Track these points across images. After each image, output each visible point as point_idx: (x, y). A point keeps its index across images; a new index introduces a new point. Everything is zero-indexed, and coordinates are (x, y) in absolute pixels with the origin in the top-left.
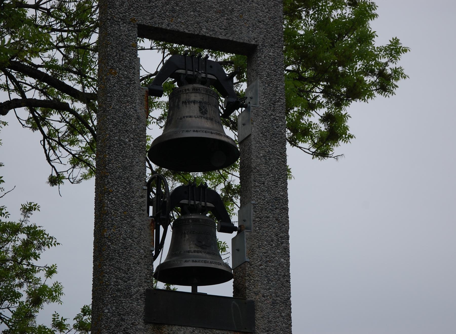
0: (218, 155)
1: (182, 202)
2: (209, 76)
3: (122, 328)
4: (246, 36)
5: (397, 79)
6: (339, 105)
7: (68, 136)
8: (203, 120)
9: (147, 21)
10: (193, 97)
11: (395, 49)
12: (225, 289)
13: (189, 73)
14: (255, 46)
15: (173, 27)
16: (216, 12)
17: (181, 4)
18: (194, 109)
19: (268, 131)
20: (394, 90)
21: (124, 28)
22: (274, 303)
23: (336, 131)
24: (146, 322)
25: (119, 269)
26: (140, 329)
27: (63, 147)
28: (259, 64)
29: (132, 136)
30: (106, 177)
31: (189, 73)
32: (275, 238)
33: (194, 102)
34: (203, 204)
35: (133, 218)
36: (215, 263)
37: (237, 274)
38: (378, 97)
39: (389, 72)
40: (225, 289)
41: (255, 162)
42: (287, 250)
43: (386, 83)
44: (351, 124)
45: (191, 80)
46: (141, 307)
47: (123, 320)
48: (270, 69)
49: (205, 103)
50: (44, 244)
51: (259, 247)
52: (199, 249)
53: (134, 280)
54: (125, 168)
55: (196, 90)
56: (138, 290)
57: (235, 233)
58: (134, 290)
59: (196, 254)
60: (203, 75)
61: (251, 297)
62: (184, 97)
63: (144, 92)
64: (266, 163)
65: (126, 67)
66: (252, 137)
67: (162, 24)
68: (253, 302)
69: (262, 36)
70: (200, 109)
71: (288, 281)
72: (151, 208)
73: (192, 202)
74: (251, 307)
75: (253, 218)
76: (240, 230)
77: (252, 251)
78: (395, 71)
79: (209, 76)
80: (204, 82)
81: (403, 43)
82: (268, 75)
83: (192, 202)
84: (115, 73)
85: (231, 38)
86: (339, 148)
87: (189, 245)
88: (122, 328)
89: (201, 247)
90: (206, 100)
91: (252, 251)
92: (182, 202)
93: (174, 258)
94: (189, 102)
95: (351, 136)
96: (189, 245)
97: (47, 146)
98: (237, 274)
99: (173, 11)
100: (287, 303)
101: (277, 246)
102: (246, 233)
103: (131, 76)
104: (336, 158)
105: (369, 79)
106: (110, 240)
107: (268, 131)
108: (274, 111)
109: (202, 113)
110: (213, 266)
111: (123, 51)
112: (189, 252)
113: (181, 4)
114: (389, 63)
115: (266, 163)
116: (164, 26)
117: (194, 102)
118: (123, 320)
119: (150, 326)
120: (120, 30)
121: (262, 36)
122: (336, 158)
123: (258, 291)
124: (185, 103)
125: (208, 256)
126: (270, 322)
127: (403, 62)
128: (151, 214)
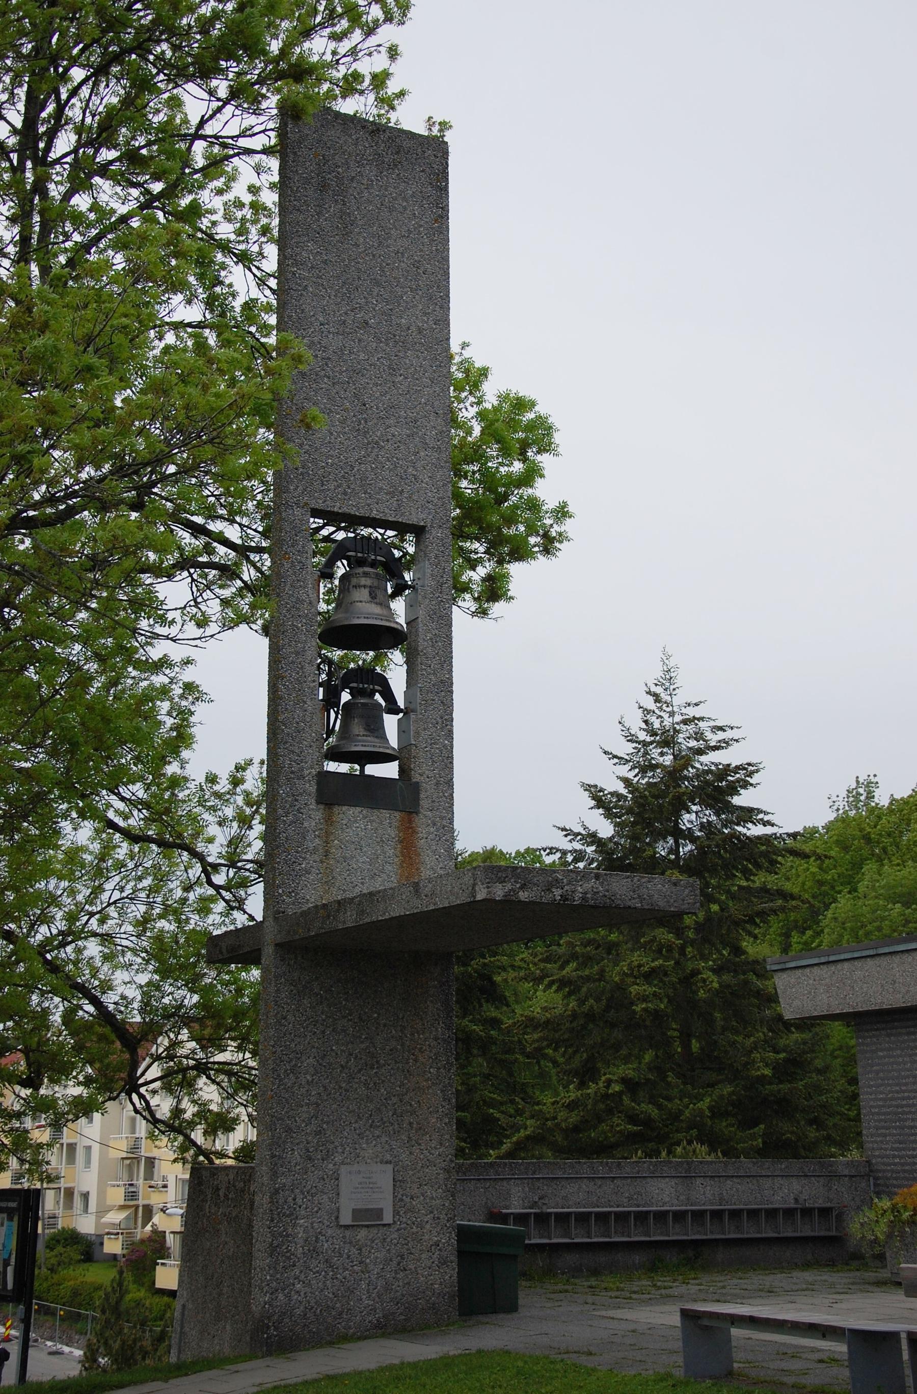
0: (384, 637)
1: (351, 685)
2: (379, 558)
3: (296, 808)
4: (414, 517)
5: (561, 542)
6: (500, 562)
7: (219, 579)
8: (373, 605)
9: (320, 505)
10: (363, 581)
11: (562, 513)
12: (389, 770)
13: (359, 555)
14: (424, 527)
15: (345, 510)
16: (386, 494)
17: (352, 487)
18: (364, 594)
19: (435, 613)
20: (557, 553)
21: (298, 512)
22: (438, 784)
23: (494, 590)
24: (318, 803)
25: (293, 752)
26: (313, 809)
27: (211, 590)
28: (427, 547)
29: (304, 621)
30: (280, 662)
31: (359, 555)
32: (440, 721)
33: (365, 586)
34: (371, 687)
35: (305, 702)
36: (383, 747)
37: (401, 756)
38: (542, 560)
39: (554, 534)
40: (389, 770)
41: (422, 644)
42: (451, 732)
43: (549, 545)
44: (514, 588)
45: (360, 563)
46: (312, 788)
47: (296, 800)
48: (438, 550)
49: (375, 587)
50: (197, 699)
51: (425, 729)
52: (368, 733)
53: (306, 763)
54: (297, 653)
55: (366, 574)
56: (310, 772)
57: (401, 715)
58: (306, 772)
59: (365, 738)
60: (373, 557)
61: (416, 778)
62: (354, 581)
63: (316, 577)
64: (433, 646)
65: (299, 551)
66: (420, 620)
67: (334, 506)
68: (418, 783)
69: (431, 517)
70: (370, 594)
71: (452, 763)
72: (321, 689)
73: (361, 686)
74: (416, 788)
75: (419, 701)
76: (406, 712)
77: (417, 733)
78: (560, 534)
79: (379, 558)
80: (373, 564)
81: (571, 509)
82: (436, 557)
83: (361, 686)
84: (289, 558)
85: (400, 520)
86: (498, 608)
87: (357, 729)
88: (296, 808)
89: (369, 730)
90: (376, 584)
91: (417, 733)
92: (351, 685)
93: (344, 742)
94: (360, 586)
95: (512, 598)
96: (357, 729)
97: (194, 589)
98: (401, 756)
99: (345, 493)
100: (450, 784)
101: (442, 728)
102: (412, 716)
103: (303, 560)
104: (496, 619)
105: (532, 540)
106: (284, 725)
107: (435, 613)
108: (441, 593)
109: (372, 598)
110: (381, 750)
111: (296, 535)
112: (358, 735)
113: (352, 487)
114: (555, 525)
115: (433, 646)
116: (336, 509)
117: (365, 586)
118: (296, 800)
119: (322, 807)
120: (294, 515)
121: (431, 517)
122: (496, 619)
123: (422, 773)
124: (355, 587)
125: (376, 740)
126: (433, 802)
127: (568, 526)
128: (321, 697)
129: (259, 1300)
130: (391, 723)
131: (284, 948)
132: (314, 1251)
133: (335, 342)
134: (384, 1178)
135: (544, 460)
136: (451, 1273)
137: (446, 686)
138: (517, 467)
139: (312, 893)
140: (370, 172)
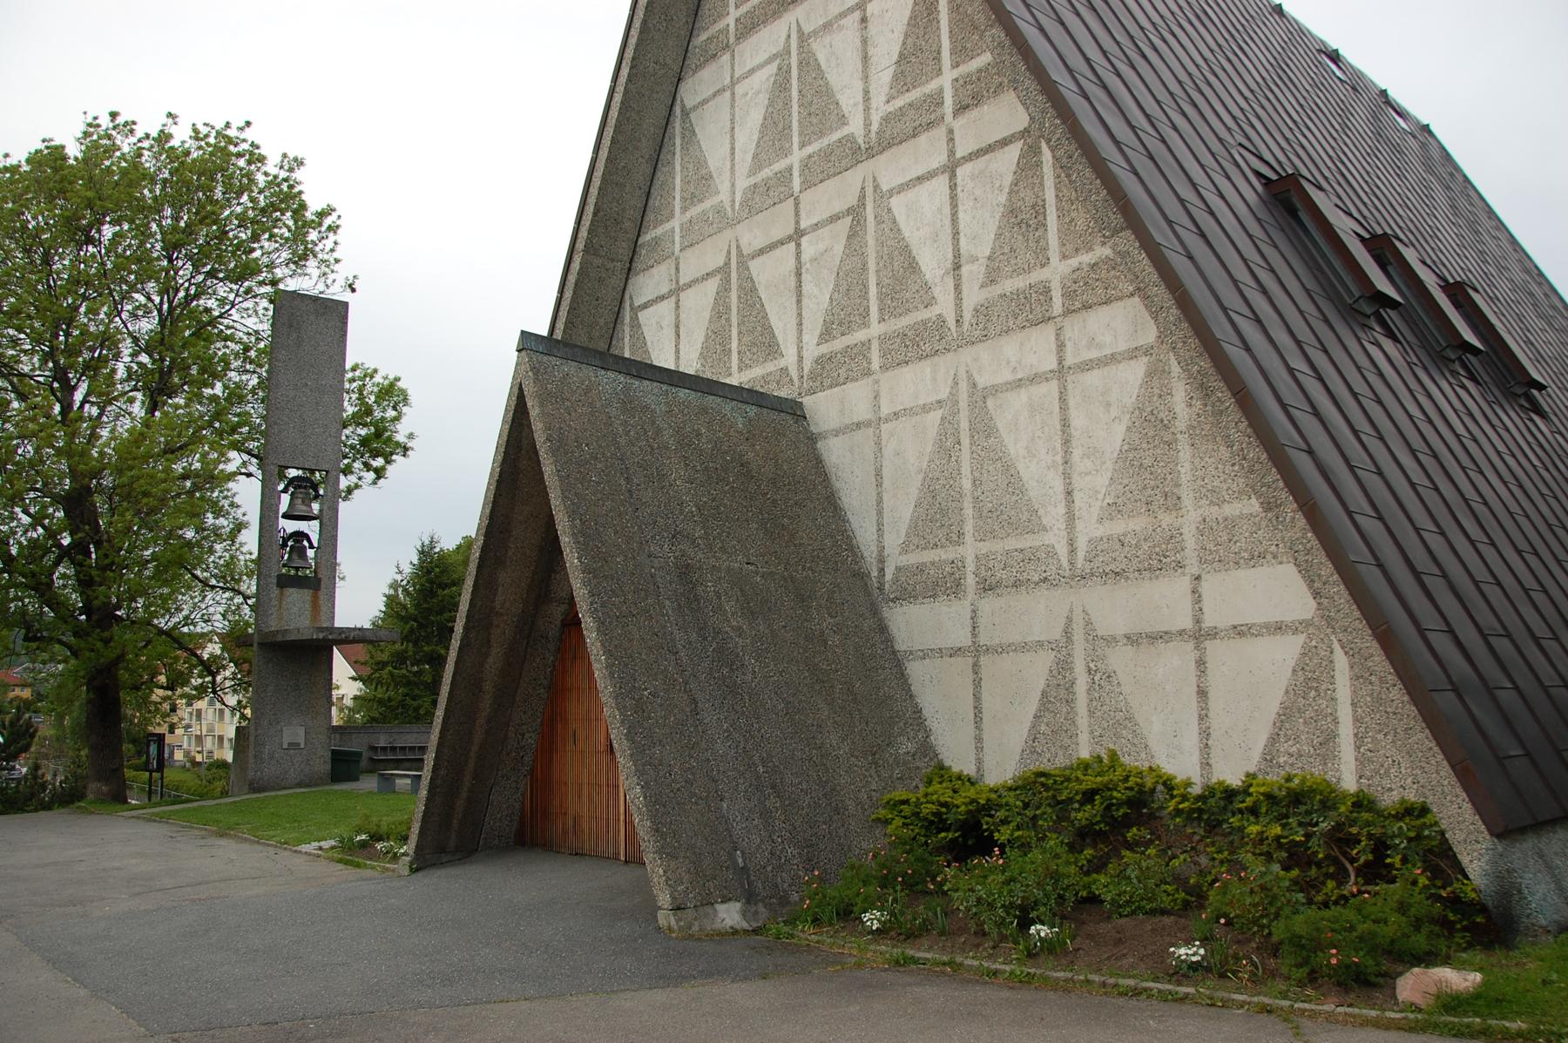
74: (319, 580)
96: (295, 557)
123: (323, 574)
129: (251, 774)
130: (311, 553)
131: (261, 645)
132: (272, 758)
133: (292, 394)
134: (301, 731)
135: (405, 409)
136: (329, 767)
137: (335, 538)
138: (394, 413)
139: (273, 625)
140: (312, 318)
